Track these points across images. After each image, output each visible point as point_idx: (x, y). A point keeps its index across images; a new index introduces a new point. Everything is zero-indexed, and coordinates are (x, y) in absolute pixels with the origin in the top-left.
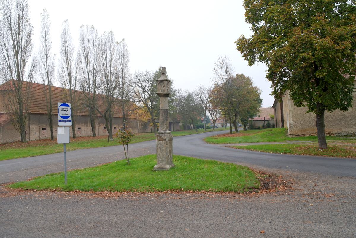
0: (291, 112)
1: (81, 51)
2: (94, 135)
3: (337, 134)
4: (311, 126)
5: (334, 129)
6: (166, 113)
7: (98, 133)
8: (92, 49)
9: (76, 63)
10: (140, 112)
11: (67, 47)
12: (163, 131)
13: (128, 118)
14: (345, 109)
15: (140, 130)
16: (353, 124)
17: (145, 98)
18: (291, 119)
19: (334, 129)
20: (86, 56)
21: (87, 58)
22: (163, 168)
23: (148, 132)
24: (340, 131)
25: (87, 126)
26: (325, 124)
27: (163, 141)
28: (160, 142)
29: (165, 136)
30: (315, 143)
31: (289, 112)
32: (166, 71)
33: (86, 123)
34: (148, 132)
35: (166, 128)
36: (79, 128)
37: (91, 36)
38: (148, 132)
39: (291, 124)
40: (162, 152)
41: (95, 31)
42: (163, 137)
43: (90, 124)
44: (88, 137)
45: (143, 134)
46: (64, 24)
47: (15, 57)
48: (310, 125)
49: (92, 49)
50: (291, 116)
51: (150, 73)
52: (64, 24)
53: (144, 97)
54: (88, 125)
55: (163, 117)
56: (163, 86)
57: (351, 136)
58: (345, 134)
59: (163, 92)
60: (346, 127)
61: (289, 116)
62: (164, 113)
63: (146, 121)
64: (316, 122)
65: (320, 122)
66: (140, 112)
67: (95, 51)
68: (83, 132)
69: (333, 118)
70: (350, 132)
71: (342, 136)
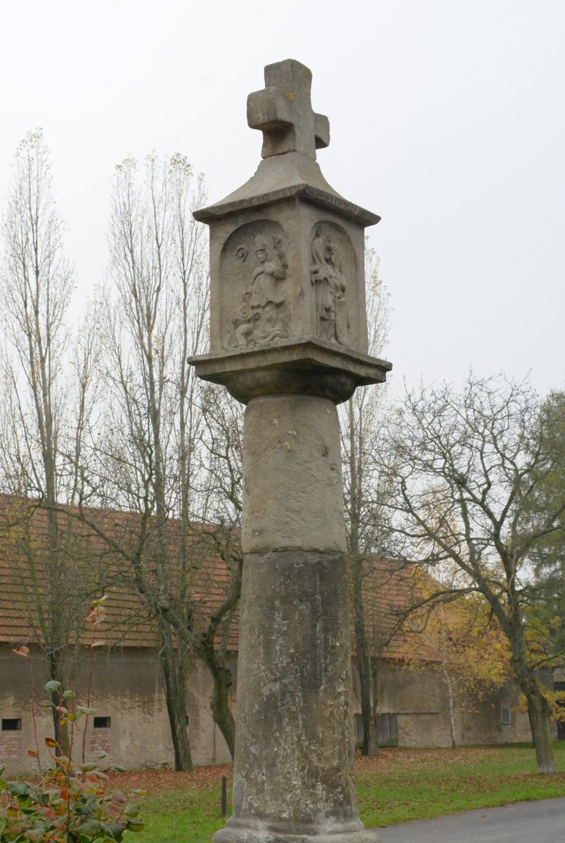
1: (115, 296)
2: (182, 762)
6: (306, 596)
7: (211, 752)
8: (173, 282)
9: (82, 357)
10: (452, 618)
11: (37, 273)
13: (386, 661)
15: (467, 728)
17: (469, 540)
20: (147, 320)
21: (150, 331)
23: (515, 741)
25: (147, 705)
32: (319, 104)
33: (141, 690)
34: (512, 745)
35: (308, 787)
36: (101, 722)
37: (169, 212)
38: (512, 745)
41: (194, 181)
43: (161, 697)
44: (151, 771)
45: (482, 753)
46: (24, 153)
49: (173, 282)
51: (491, 386)
52: (24, 153)
53: (467, 535)
54: (152, 701)
55: (268, 644)
56: (271, 266)
59: (262, 344)
62: (286, 600)
63: (495, 679)
66: (452, 618)
67: (189, 290)
68: (125, 743)
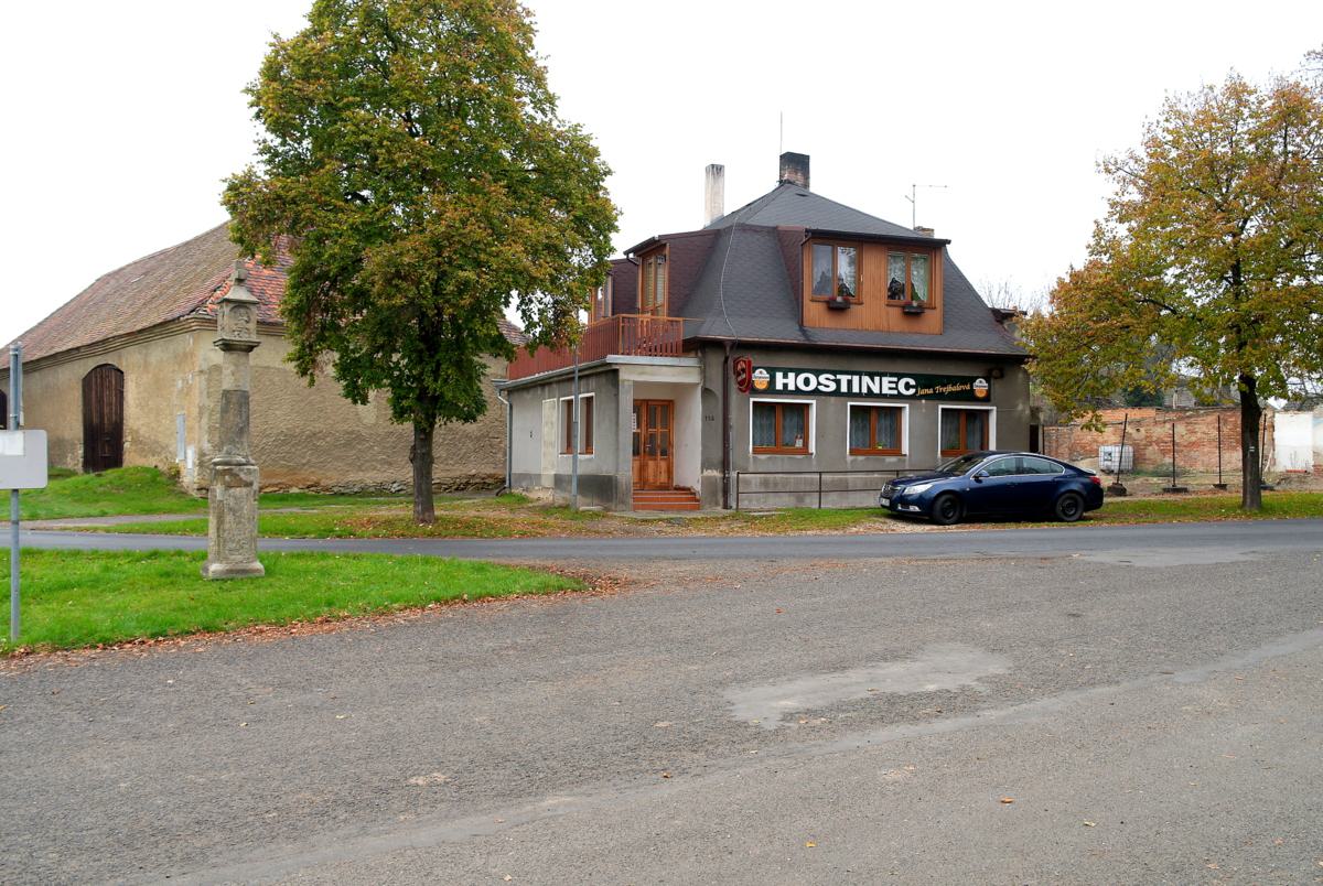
0: (206, 415)
3: (335, 490)
4: (265, 461)
5: (329, 474)
12: (240, 459)
14: (469, 418)
16: (376, 460)
18: (206, 437)
19: (329, 474)
22: (244, 571)
24: (346, 480)
26: (435, 453)
27: (244, 490)
28: (232, 490)
29: (250, 473)
30: (404, 511)
31: (201, 414)
39: (204, 455)
40: (240, 522)
42: (242, 475)
47: (1261, 427)
48: (263, 457)
50: (206, 427)
57: (371, 494)
58: (356, 490)
60: (360, 469)
61: (200, 427)
64: (414, 448)
65: (424, 451)
69: (328, 439)
70: (369, 482)
71: (350, 495)
